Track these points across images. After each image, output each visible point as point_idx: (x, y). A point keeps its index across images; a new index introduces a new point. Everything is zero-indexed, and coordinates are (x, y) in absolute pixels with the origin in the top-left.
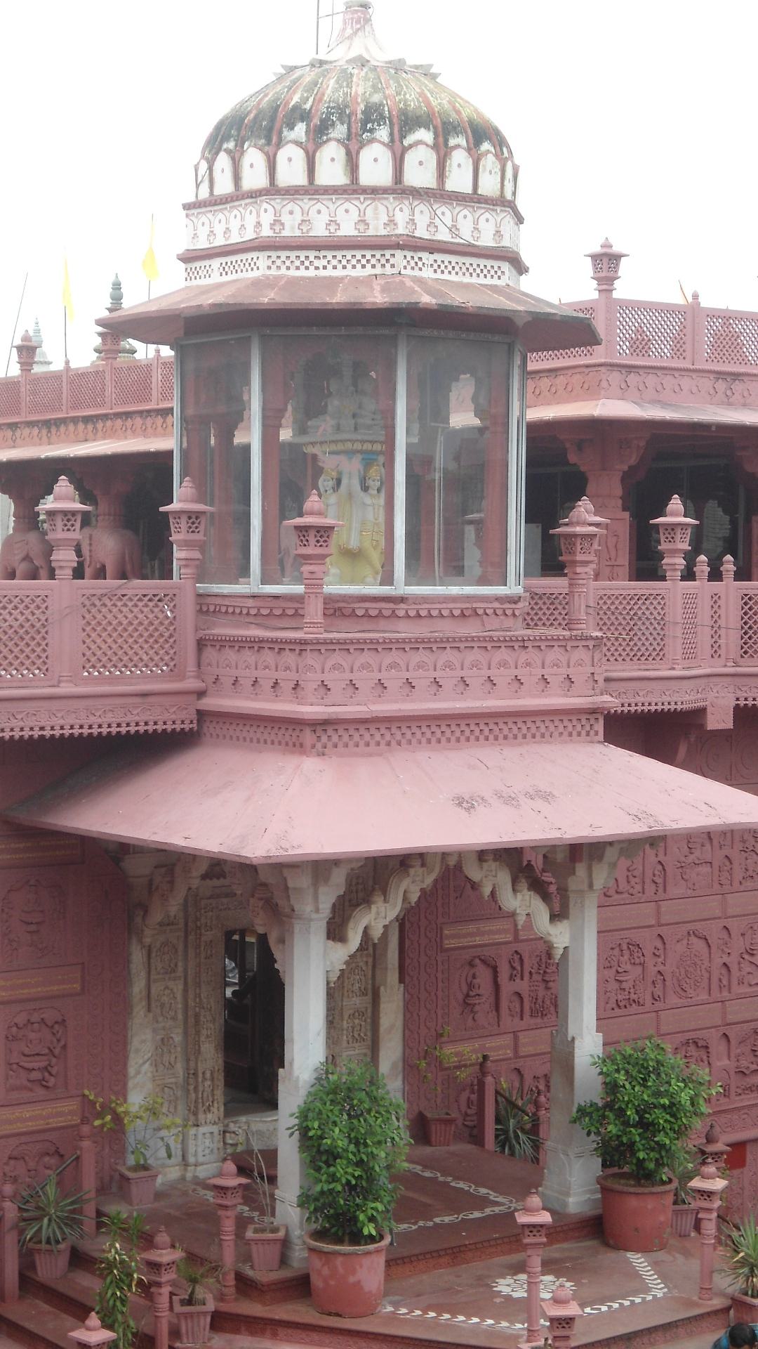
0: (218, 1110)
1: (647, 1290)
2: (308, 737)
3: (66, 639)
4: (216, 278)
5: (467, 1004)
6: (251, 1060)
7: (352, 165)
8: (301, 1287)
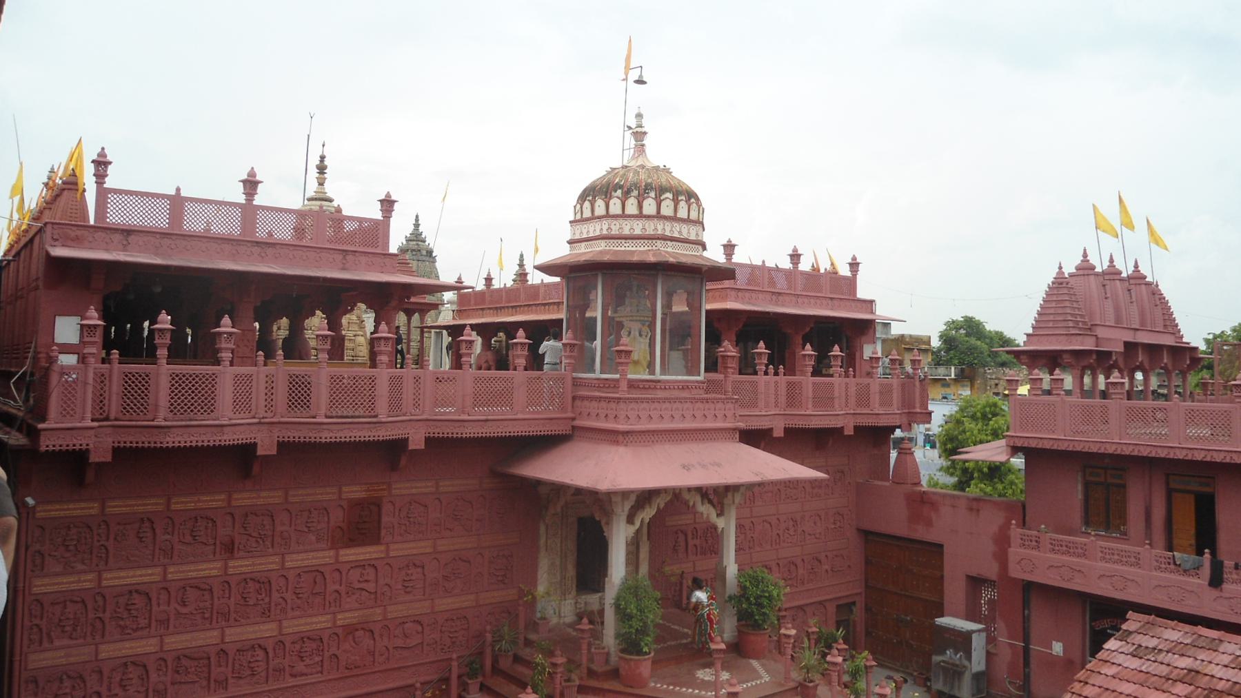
0: (574, 593)
1: (761, 678)
2: (620, 438)
3: (520, 396)
4: (583, 250)
5: (675, 550)
6: (590, 571)
7: (640, 207)
8: (615, 674)
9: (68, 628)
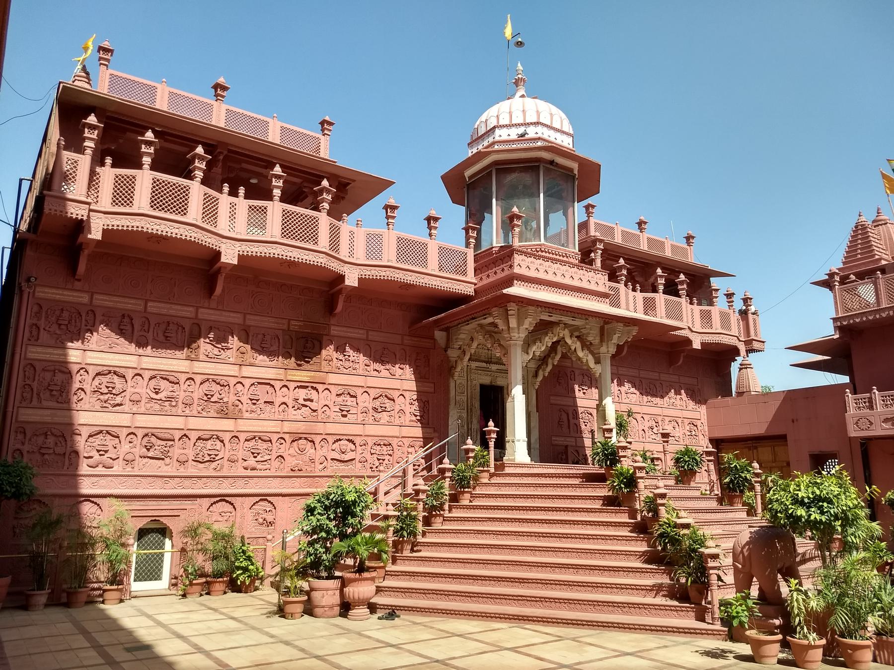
9: (54, 393)
